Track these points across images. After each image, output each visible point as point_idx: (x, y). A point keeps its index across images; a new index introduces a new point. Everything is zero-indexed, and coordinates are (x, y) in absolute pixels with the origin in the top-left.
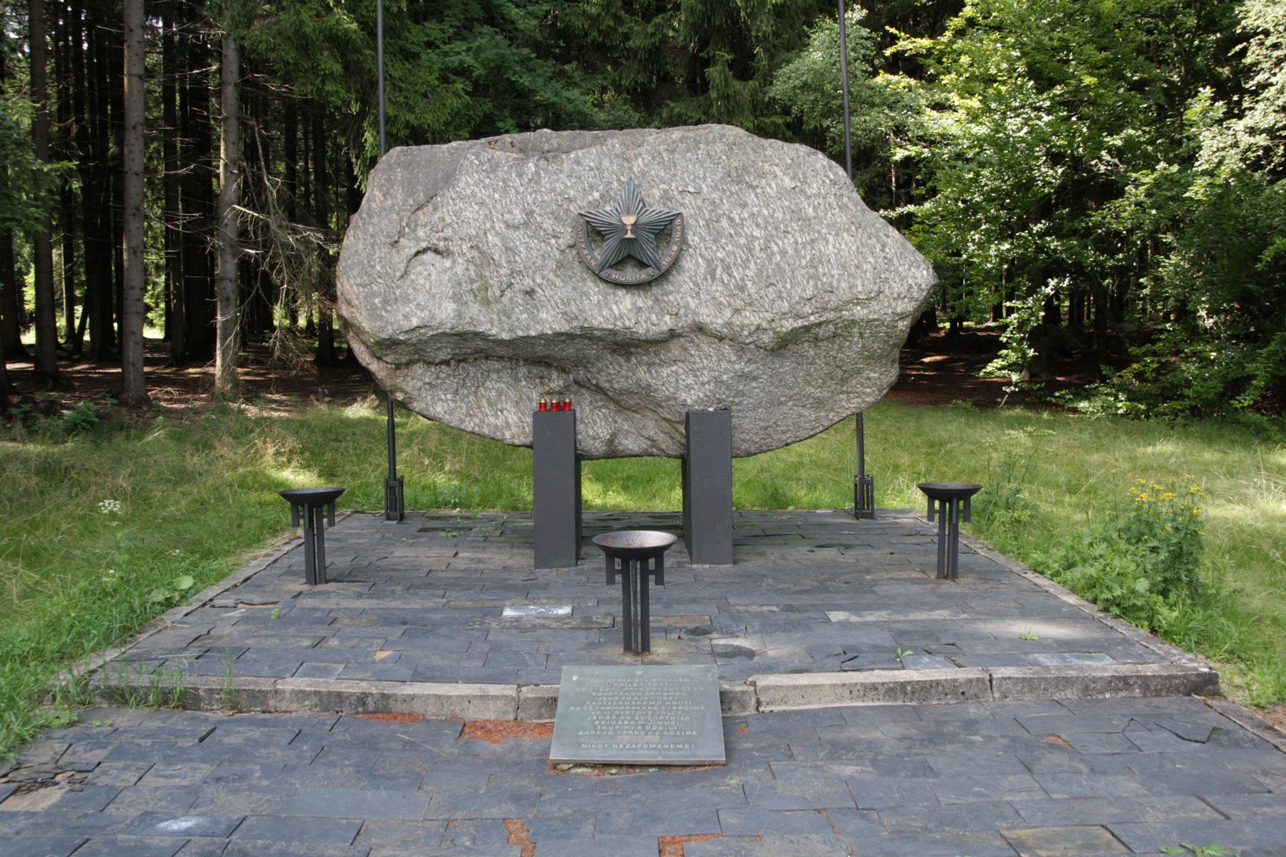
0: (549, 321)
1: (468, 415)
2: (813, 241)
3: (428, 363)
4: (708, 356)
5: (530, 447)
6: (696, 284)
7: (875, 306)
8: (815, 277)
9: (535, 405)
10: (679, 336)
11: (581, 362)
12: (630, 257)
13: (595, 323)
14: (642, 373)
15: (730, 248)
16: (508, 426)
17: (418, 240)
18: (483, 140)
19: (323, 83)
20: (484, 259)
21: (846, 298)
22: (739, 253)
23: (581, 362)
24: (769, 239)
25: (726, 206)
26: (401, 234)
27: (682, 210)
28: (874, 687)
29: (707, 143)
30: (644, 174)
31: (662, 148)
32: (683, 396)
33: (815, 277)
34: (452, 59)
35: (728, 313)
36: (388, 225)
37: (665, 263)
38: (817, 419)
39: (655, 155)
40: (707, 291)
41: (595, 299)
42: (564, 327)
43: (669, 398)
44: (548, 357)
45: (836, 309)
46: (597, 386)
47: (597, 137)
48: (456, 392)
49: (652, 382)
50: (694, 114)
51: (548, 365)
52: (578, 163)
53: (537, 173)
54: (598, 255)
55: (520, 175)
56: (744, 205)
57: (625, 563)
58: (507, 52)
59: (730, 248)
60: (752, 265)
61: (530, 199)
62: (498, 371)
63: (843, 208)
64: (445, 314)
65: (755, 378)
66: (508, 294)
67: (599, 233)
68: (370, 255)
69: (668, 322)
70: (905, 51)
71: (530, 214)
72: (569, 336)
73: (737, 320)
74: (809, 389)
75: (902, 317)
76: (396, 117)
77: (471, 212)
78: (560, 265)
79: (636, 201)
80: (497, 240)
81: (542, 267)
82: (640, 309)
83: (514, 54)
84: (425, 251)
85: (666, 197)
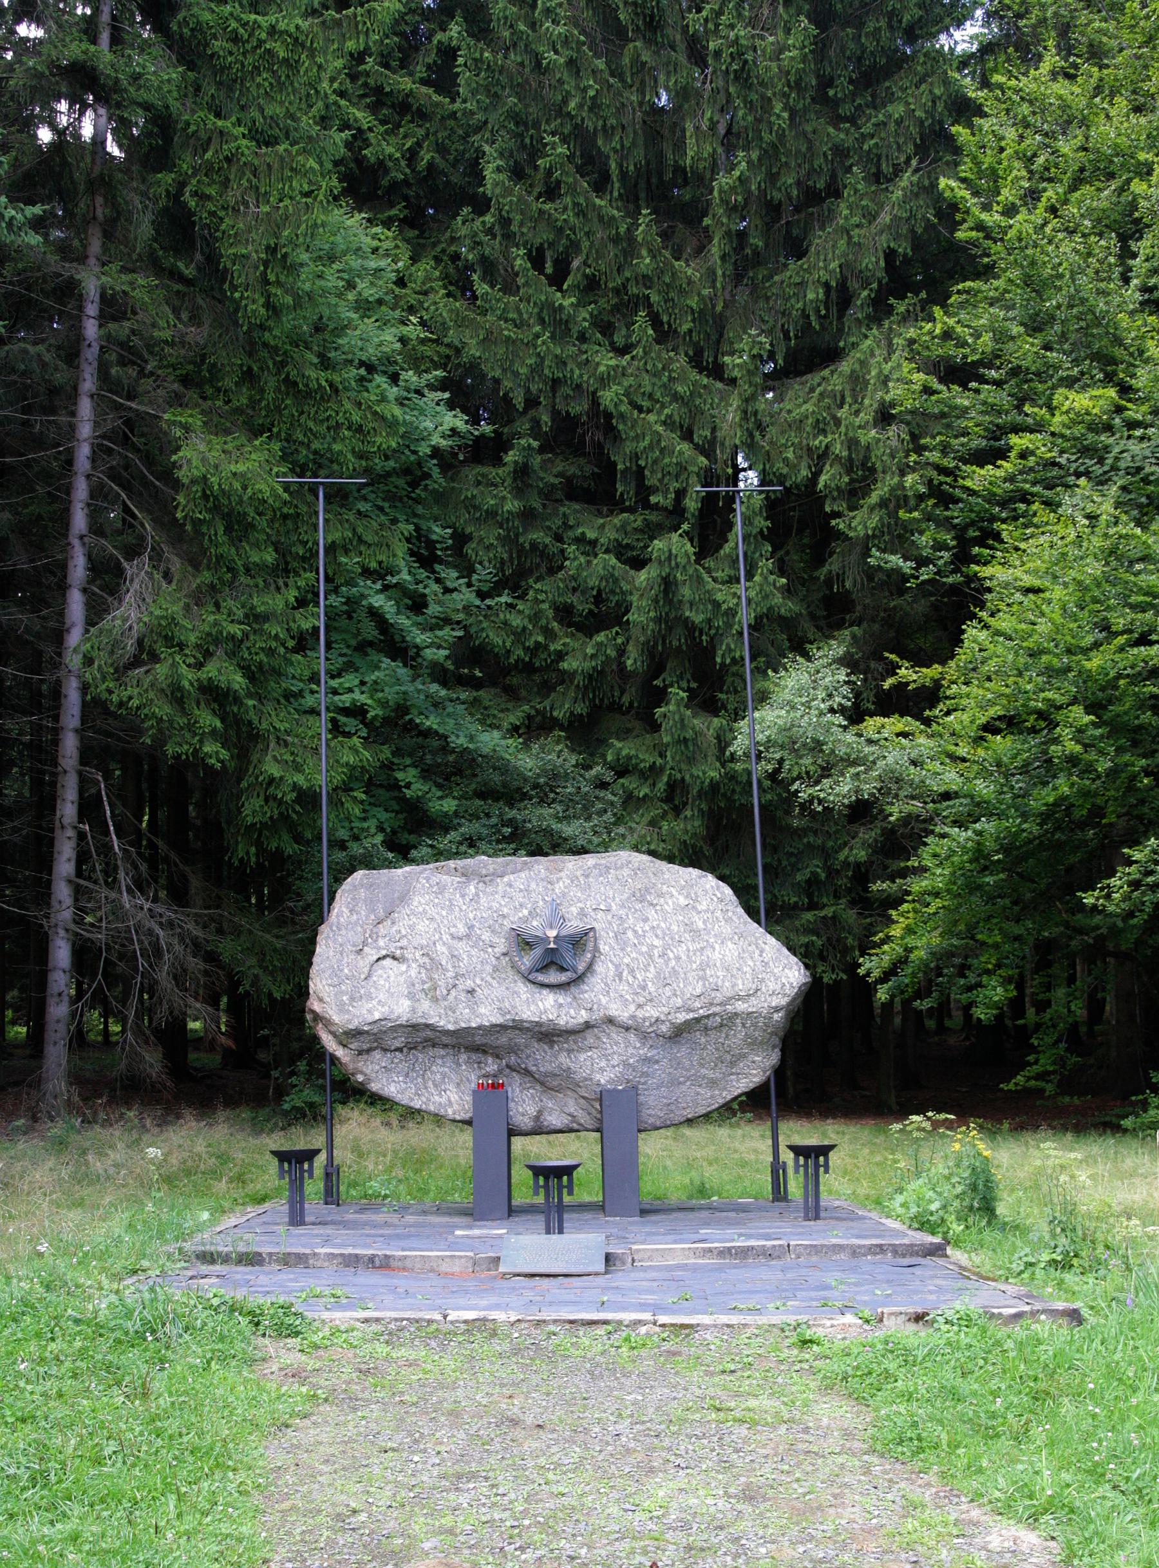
0: (487, 1014)
1: (417, 1094)
2: (702, 949)
3: (385, 1050)
4: (617, 1043)
5: (469, 1123)
6: (606, 984)
7: (753, 1001)
8: (703, 978)
9: (473, 1086)
10: (593, 1026)
11: (513, 1050)
12: (552, 963)
13: (525, 1017)
14: (563, 1059)
15: (634, 955)
16: (450, 1104)
17: (379, 948)
18: (431, 866)
19: (201, 742)
20: (435, 965)
21: (729, 995)
22: (641, 959)
23: (513, 1050)
24: (666, 947)
25: (631, 921)
26: (365, 943)
27: (595, 925)
28: (710, 1250)
29: (616, 869)
30: (564, 895)
31: (579, 873)
32: (598, 1077)
33: (703, 978)
34: (343, 698)
35: (632, 1008)
36: (353, 936)
37: (581, 967)
38: (712, 1097)
39: (573, 879)
40: (616, 991)
41: (524, 997)
42: (499, 1020)
43: (586, 1079)
44: (485, 1045)
45: (720, 1005)
46: (526, 1070)
47: (525, 863)
48: (407, 1075)
49: (572, 1065)
50: (647, 757)
51: (485, 1052)
52: (510, 886)
53: (477, 895)
54: (527, 961)
55: (463, 896)
56: (646, 920)
57: (546, 1178)
58: (409, 688)
59: (634, 955)
60: (652, 969)
61: (471, 916)
62: (443, 1057)
63: (728, 920)
64: (402, 1009)
65: (657, 1062)
66: (453, 993)
67: (528, 943)
68: (339, 961)
69: (583, 1016)
70: (907, 684)
71: (471, 927)
72: (502, 1028)
73: (640, 1014)
74: (704, 1071)
75: (777, 1009)
76: (281, 778)
77: (422, 926)
78: (496, 969)
79: (556, 916)
80: (444, 949)
81: (482, 971)
82: (561, 1005)
83: (419, 691)
84: (384, 957)
85: (582, 914)
